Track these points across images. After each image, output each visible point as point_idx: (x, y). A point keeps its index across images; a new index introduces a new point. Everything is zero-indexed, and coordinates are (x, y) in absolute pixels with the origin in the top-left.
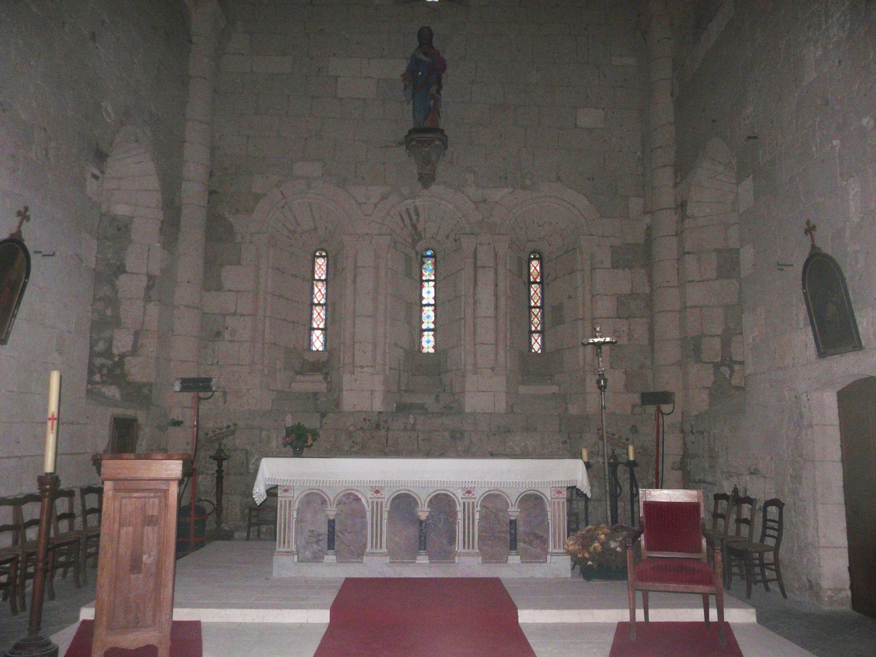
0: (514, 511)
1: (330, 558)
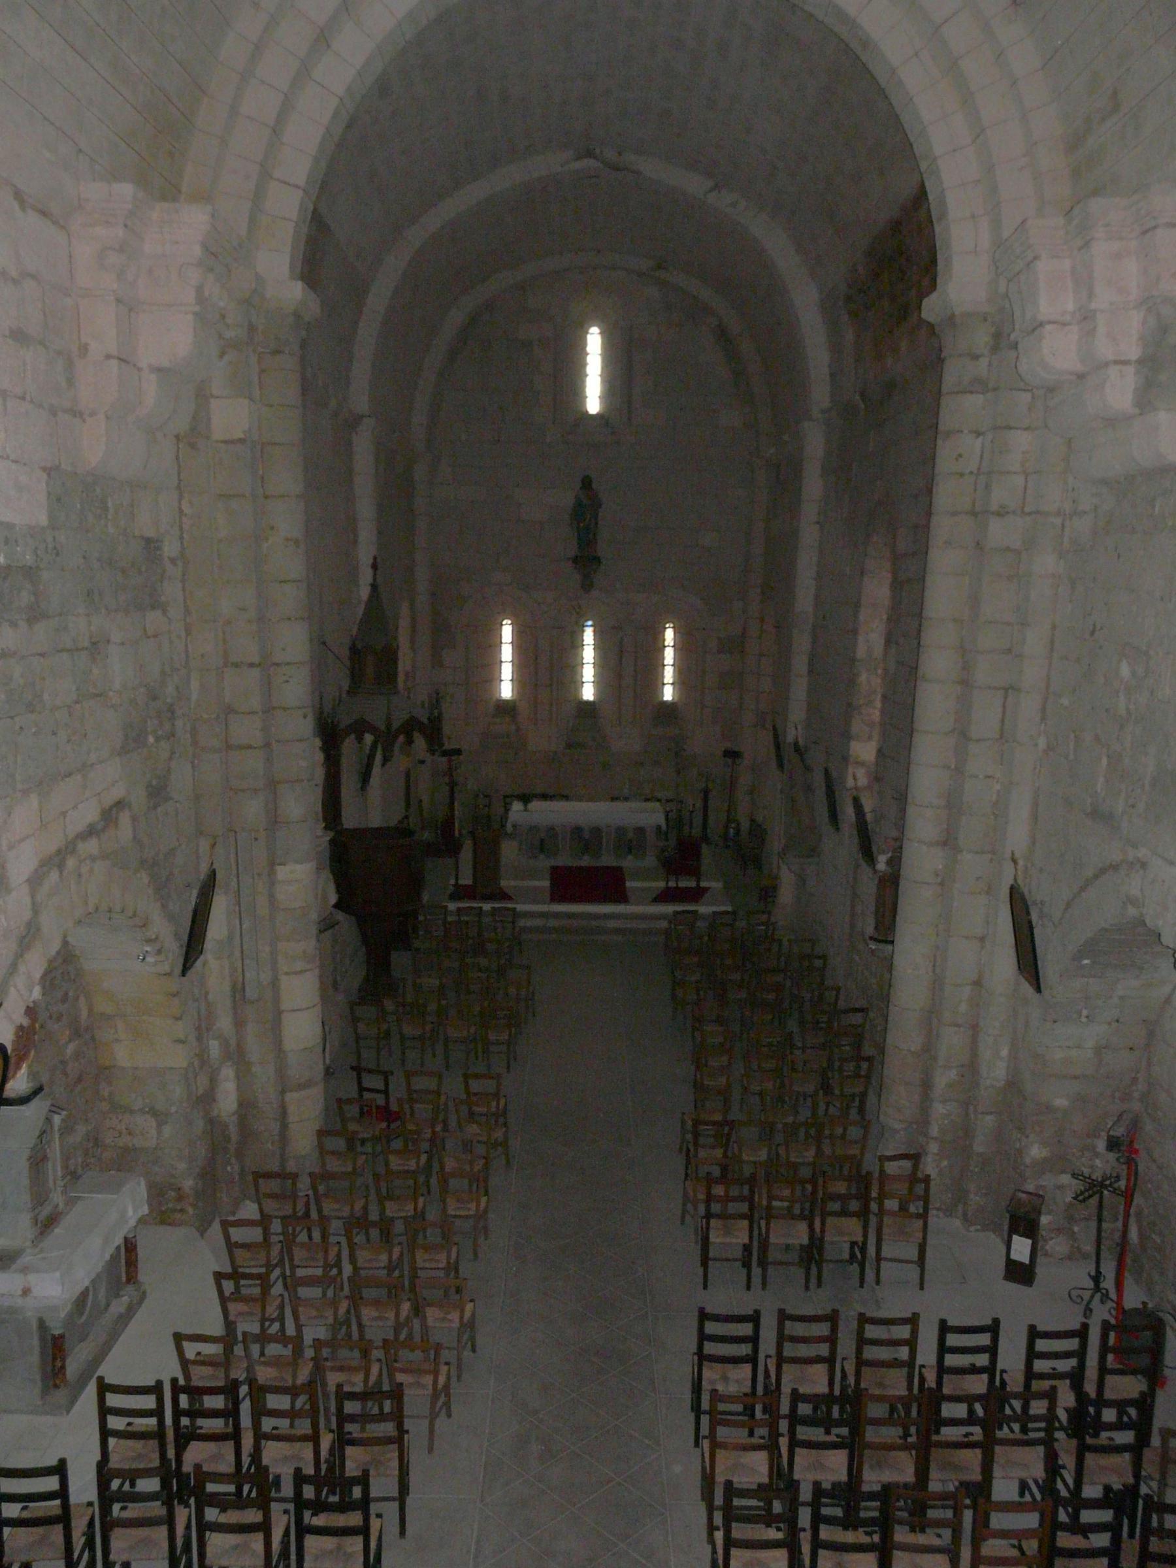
0: (630, 835)
1: (542, 857)
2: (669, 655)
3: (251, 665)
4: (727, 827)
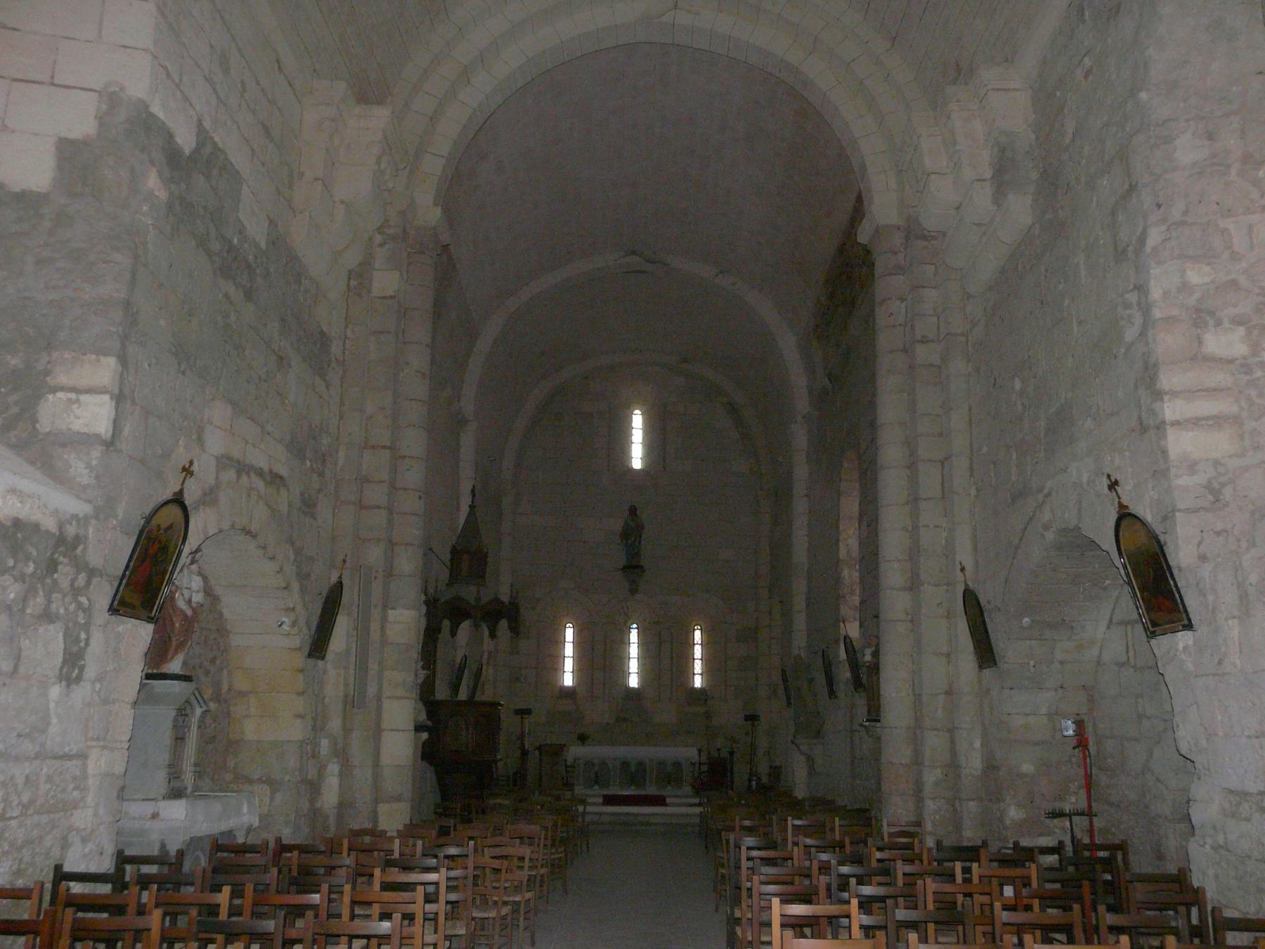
1: (596, 787)
2: (698, 651)
3: (384, 447)
4: (750, 781)
